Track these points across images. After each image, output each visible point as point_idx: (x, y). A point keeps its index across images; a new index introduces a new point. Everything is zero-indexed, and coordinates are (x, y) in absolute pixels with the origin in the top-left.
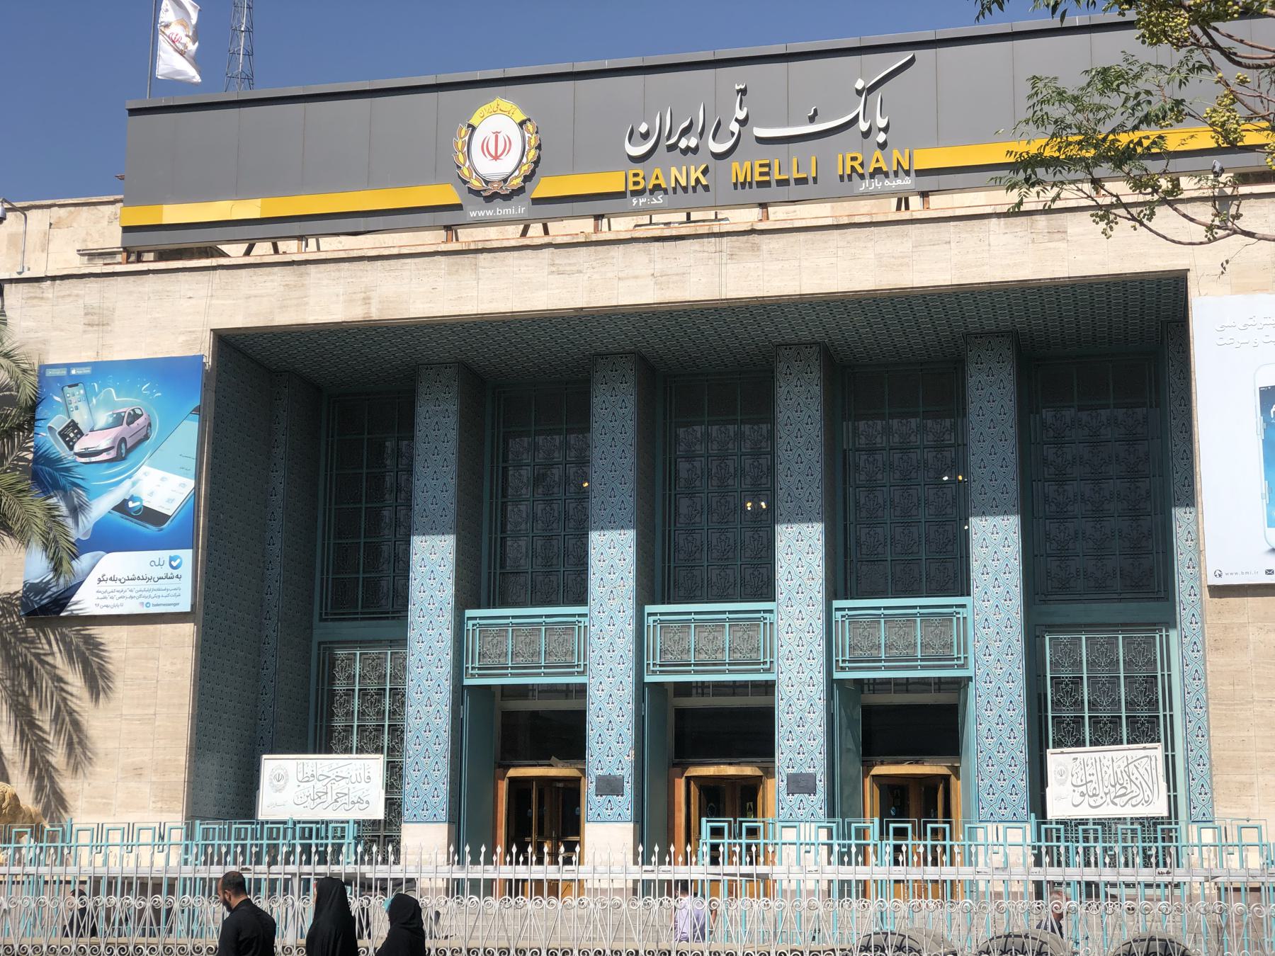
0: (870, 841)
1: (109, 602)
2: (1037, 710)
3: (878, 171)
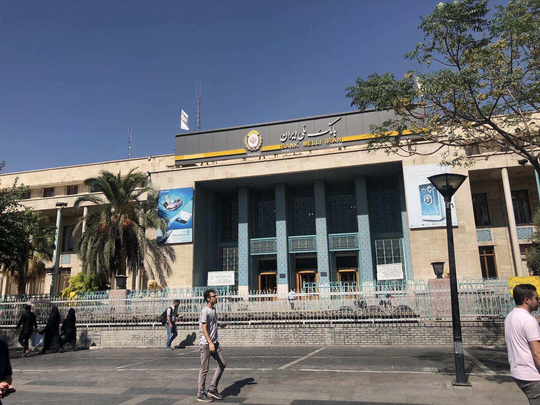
1: (175, 240)
3: (334, 142)
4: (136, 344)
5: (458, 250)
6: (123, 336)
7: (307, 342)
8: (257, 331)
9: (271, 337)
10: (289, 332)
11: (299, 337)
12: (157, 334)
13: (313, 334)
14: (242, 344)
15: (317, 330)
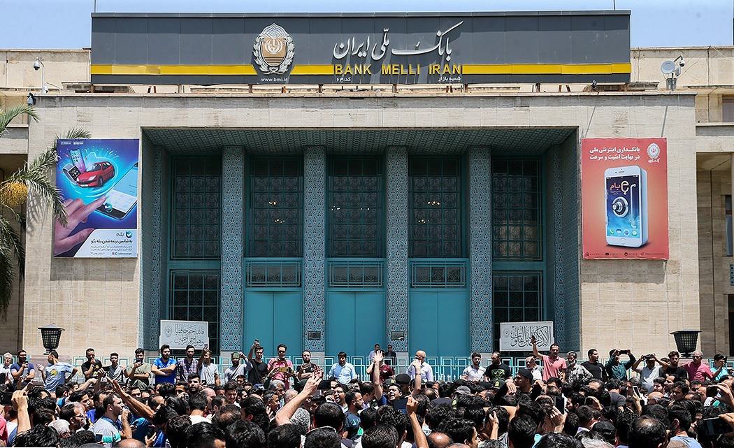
1: (98, 252)
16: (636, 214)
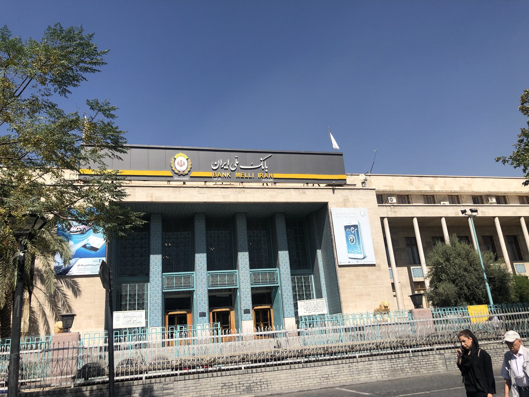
0: (218, 328)
2: (116, 302)
3: (266, 177)
4: (227, 394)
5: (377, 286)
6: (207, 386)
7: (422, 371)
8: (371, 364)
9: (387, 369)
10: (403, 362)
11: (414, 366)
12: (255, 378)
13: (426, 362)
14: (359, 380)
15: (428, 358)
16: (359, 243)
